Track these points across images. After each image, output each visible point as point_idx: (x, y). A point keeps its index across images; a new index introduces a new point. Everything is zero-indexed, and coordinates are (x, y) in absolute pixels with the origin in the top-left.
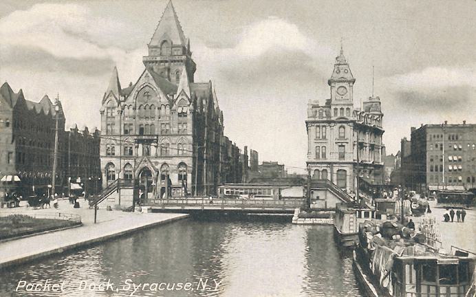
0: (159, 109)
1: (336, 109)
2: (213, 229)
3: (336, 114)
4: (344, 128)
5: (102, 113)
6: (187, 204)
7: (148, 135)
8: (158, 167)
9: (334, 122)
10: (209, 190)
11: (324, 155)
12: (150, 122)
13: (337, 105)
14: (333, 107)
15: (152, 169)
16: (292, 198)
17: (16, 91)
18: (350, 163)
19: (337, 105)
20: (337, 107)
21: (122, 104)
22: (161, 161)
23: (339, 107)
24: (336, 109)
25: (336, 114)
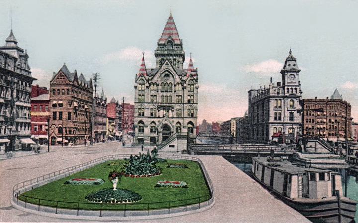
0: (175, 86)
1: (288, 89)
2: (11, 76)
3: (288, 92)
4: (293, 101)
5: (136, 87)
6: (224, 150)
7: (166, 103)
8: (174, 124)
9: (286, 97)
10: (279, 109)
11: (280, 118)
12: (168, 94)
13: (289, 86)
14: (286, 88)
15: (170, 125)
16: (210, 154)
17: (71, 71)
18: (297, 123)
19: (289, 86)
20: (293, 87)
21: (150, 82)
22: (176, 120)
23: (290, 88)
24: (288, 89)
25: (288, 92)
